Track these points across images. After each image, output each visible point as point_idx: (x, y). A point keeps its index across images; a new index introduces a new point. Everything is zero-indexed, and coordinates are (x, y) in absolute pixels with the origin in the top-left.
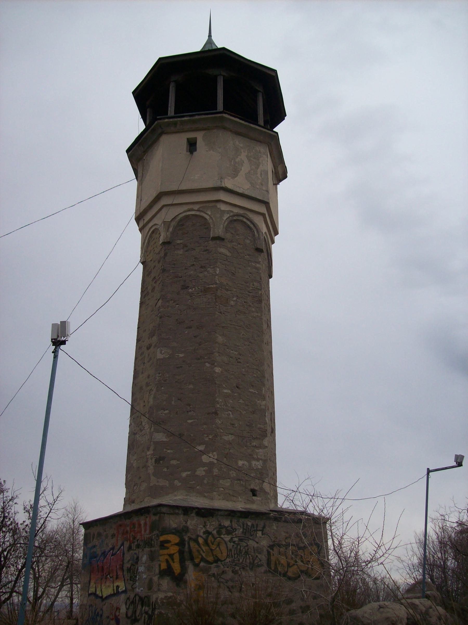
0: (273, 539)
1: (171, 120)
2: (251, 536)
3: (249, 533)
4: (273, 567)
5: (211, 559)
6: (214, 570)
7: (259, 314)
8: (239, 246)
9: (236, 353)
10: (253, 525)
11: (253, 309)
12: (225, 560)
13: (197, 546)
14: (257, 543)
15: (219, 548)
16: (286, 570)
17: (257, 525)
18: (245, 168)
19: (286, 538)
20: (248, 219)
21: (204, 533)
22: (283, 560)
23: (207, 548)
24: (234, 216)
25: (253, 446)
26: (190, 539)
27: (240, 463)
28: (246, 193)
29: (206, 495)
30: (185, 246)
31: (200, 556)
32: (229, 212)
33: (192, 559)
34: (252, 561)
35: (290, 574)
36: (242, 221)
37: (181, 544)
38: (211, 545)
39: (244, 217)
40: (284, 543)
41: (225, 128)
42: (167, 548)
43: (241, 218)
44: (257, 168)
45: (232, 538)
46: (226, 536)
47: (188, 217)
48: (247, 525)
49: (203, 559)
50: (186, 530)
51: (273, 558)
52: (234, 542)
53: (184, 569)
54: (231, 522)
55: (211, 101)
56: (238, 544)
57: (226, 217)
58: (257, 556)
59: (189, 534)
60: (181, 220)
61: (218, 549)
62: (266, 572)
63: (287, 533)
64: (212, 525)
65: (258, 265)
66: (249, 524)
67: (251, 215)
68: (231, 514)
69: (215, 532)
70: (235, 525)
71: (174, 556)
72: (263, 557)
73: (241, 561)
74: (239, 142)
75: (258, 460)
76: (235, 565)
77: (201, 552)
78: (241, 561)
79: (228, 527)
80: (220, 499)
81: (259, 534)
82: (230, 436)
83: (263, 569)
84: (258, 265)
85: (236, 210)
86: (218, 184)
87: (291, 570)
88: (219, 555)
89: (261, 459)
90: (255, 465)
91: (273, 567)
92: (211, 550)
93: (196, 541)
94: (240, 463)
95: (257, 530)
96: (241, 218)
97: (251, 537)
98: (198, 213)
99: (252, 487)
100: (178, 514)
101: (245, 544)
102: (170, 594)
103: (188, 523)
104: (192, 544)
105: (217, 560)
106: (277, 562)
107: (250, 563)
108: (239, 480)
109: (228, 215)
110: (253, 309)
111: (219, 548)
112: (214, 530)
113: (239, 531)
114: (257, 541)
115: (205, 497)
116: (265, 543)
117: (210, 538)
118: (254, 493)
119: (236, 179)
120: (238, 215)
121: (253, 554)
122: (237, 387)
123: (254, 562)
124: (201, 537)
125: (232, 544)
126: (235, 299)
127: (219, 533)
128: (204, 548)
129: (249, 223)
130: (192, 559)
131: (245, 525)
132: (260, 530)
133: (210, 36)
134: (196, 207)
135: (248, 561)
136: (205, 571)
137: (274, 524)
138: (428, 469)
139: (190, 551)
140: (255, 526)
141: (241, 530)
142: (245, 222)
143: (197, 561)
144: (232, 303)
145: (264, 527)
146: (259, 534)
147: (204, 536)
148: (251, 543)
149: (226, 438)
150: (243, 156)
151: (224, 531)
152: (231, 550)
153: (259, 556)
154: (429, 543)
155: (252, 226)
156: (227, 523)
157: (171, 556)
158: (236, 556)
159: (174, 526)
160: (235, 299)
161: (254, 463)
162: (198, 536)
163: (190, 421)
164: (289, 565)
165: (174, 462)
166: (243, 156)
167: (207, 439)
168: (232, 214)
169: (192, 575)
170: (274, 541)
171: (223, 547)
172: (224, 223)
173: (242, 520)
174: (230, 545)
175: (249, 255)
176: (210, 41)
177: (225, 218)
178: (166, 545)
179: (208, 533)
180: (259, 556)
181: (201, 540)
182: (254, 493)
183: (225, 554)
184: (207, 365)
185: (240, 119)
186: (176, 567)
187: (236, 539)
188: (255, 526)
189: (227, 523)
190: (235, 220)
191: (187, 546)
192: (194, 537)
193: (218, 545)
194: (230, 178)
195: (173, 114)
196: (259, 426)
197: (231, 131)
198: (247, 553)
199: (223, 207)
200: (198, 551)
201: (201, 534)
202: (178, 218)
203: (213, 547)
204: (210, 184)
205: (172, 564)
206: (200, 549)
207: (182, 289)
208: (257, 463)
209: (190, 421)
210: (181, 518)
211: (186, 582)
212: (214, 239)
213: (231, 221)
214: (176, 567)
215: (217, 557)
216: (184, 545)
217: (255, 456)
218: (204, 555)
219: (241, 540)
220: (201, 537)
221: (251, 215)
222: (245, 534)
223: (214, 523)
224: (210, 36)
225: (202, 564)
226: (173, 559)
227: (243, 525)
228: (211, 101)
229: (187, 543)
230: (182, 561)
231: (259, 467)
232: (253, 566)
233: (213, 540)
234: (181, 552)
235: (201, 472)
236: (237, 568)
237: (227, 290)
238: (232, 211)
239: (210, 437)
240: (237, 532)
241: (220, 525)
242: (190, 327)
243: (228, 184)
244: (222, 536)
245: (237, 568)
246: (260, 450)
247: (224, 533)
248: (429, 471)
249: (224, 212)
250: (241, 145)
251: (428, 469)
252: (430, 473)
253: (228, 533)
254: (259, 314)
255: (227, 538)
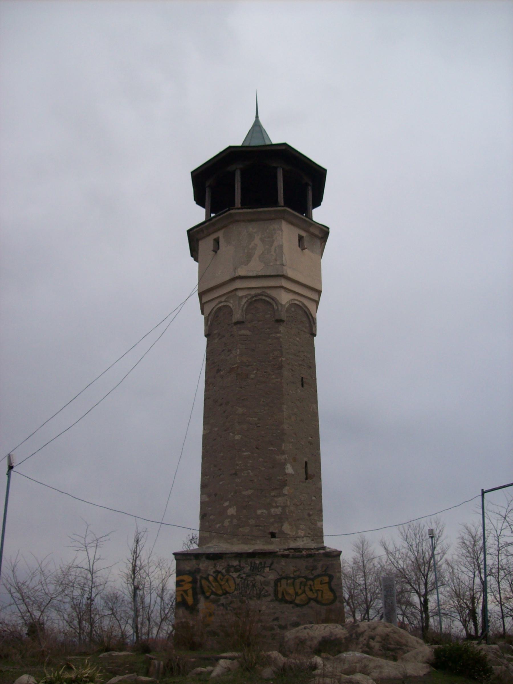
0: (280, 573)
1: (198, 228)
2: (259, 572)
3: (256, 569)
4: (280, 596)
5: (220, 592)
6: (223, 600)
7: (279, 380)
8: (260, 323)
9: (256, 419)
10: (261, 563)
11: (273, 377)
12: (233, 592)
13: (207, 583)
14: (265, 577)
15: (228, 583)
16: (294, 598)
17: (265, 563)
18: (258, 252)
19: (295, 571)
20: (265, 296)
21: (214, 572)
22: (291, 591)
23: (217, 583)
24: (253, 297)
25: (272, 496)
26: (202, 578)
27: (259, 512)
28: (260, 274)
29: (229, 541)
30: (219, 334)
31: (210, 591)
32: (246, 296)
33: (203, 593)
34: (258, 592)
35: (297, 601)
36: (262, 300)
37: (194, 582)
38: (220, 581)
39: (262, 295)
40: (292, 576)
41: (237, 221)
42: (182, 586)
43: (260, 297)
44: (272, 245)
45: (239, 575)
46: (234, 573)
47: (220, 309)
48: (255, 563)
49: (213, 593)
50: (198, 571)
51: (280, 589)
52: (242, 578)
53: (196, 601)
54: (240, 562)
55: (259, 187)
56: (245, 580)
57: (244, 300)
58: (264, 588)
59: (201, 574)
60: (216, 313)
61: (226, 584)
62: (272, 601)
63: (296, 567)
64: (221, 566)
65: (278, 335)
66: (258, 562)
67: (269, 292)
68: (239, 556)
69: (224, 571)
70: (243, 564)
71: (188, 591)
72: (270, 589)
73: (248, 592)
74: (252, 228)
75: (277, 507)
76: (243, 596)
77: (212, 587)
78: (248, 592)
79: (236, 566)
80: (239, 544)
81: (267, 570)
82: (250, 490)
83: (269, 598)
84: (278, 335)
85: (253, 292)
86: (233, 276)
87: (298, 598)
88: (228, 589)
89: (281, 506)
90: (274, 511)
91: (280, 596)
92: (221, 585)
93: (207, 579)
94: (259, 512)
95: (265, 567)
96: (260, 297)
97: (258, 573)
98: (225, 304)
99: (271, 531)
100: (191, 560)
101: (253, 579)
102: (183, 620)
103: (201, 565)
104: (204, 582)
105: (226, 593)
106: (285, 592)
107: (257, 594)
108: (257, 526)
109: (246, 299)
110: (273, 377)
111: (228, 583)
112: (223, 569)
113: (247, 569)
114: (264, 575)
115: (228, 543)
116: (272, 577)
117: (220, 576)
118: (273, 535)
119: (249, 264)
120: (256, 295)
121: (260, 586)
122: (257, 448)
123: (260, 593)
124: (212, 575)
125: (240, 579)
126: (255, 372)
127: (228, 571)
128: (214, 584)
129: (267, 299)
130: (203, 593)
131: (253, 564)
132: (268, 567)
133: (257, 117)
134: (223, 299)
135: (255, 592)
136: (215, 602)
137: (282, 560)
138: (482, 490)
139: (202, 587)
140: (263, 563)
141: (249, 568)
142: (264, 300)
143: (208, 594)
144: (252, 376)
145: (272, 564)
146: (267, 570)
147: (214, 575)
148: (259, 578)
149: (245, 493)
150: (257, 241)
151: (232, 569)
152: (238, 584)
153: (266, 588)
154: (166, 594)
155: (271, 301)
156: (235, 563)
157: (186, 591)
158: (243, 589)
159: (188, 568)
160: (255, 372)
161: (272, 510)
162: (209, 575)
163: (221, 483)
164: (297, 594)
165: (212, 517)
166: (257, 241)
167: (230, 496)
168: (249, 297)
169: (202, 604)
170: (281, 575)
171: (231, 582)
172: (243, 307)
173: (249, 560)
174: (238, 580)
175: (269, 328)
176: (257, 127)
177: (243, 303)
178: (181, 583)
179: (218, 572)
180: (266, 588)
181: (211, 578)
182: (273, 535)
183: (233, 588)
184: (231, 434)
185: (247, 208)
186: (190, 600)
187: (244, 576)
188: (263, 563)
189: (235, 563)
190: (255, 301)
191: (198, 583)
192: (204, 576)
193: (227, 581)
194: (243, 266)
195: (240, 206)
196: (278, 478)
197: (244, 221)
198: (254, 586)
199: (240, 294)
200: (208, 586)
201: (212, 573)
202: (213, 312)
203: (222, 583)
204: (227, 278)
205: (186, 597)
206: (210, 585)
207: (217, 372)
208: (277, 510)
209: (221, 483)
210: (194, 562)
211: (198, 611)
212: (237, 323)
213: (251, 303)
214: (190, 600)
215: (225, 590)
216: (196, 582)
217: (274, 504)
218: (214, 589)
219: (248, 576)
220: (212, 575)
221: (269, 292)
222: (253, 571)
223: (223, 564)
224: (257, 117)
225: (212, 596)
226: (187, 595)
227: (251, 563)
228: (259, 187)
229: (198, 581)
230: (195, 594)
231: (278, 513)
232: (259, 597)
233: (222, 577)
234: (194, 589)
235: (227, 523)
236: (244, 598)
237: (248, 366)
238: (250, 294)
239: (232, 494)
240: (245, 570)
241: (228, 565)
242: (221, 405)
243: (241, 272)
244: (231, 574)
245: (244, 598)
246: (280, 498)
247: (233, 571)
248: (483, 492)
249: (242, 297)
250: (255, 230)
251: (482, 490)
252: (485, 494)
253: (236, 571)
254: (279, 380)
255: (235, 575)
